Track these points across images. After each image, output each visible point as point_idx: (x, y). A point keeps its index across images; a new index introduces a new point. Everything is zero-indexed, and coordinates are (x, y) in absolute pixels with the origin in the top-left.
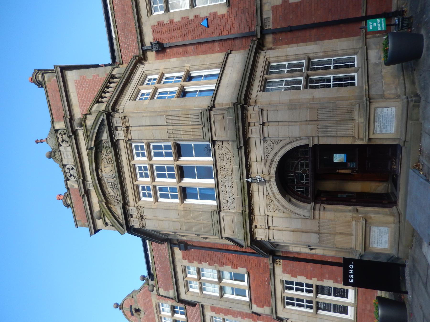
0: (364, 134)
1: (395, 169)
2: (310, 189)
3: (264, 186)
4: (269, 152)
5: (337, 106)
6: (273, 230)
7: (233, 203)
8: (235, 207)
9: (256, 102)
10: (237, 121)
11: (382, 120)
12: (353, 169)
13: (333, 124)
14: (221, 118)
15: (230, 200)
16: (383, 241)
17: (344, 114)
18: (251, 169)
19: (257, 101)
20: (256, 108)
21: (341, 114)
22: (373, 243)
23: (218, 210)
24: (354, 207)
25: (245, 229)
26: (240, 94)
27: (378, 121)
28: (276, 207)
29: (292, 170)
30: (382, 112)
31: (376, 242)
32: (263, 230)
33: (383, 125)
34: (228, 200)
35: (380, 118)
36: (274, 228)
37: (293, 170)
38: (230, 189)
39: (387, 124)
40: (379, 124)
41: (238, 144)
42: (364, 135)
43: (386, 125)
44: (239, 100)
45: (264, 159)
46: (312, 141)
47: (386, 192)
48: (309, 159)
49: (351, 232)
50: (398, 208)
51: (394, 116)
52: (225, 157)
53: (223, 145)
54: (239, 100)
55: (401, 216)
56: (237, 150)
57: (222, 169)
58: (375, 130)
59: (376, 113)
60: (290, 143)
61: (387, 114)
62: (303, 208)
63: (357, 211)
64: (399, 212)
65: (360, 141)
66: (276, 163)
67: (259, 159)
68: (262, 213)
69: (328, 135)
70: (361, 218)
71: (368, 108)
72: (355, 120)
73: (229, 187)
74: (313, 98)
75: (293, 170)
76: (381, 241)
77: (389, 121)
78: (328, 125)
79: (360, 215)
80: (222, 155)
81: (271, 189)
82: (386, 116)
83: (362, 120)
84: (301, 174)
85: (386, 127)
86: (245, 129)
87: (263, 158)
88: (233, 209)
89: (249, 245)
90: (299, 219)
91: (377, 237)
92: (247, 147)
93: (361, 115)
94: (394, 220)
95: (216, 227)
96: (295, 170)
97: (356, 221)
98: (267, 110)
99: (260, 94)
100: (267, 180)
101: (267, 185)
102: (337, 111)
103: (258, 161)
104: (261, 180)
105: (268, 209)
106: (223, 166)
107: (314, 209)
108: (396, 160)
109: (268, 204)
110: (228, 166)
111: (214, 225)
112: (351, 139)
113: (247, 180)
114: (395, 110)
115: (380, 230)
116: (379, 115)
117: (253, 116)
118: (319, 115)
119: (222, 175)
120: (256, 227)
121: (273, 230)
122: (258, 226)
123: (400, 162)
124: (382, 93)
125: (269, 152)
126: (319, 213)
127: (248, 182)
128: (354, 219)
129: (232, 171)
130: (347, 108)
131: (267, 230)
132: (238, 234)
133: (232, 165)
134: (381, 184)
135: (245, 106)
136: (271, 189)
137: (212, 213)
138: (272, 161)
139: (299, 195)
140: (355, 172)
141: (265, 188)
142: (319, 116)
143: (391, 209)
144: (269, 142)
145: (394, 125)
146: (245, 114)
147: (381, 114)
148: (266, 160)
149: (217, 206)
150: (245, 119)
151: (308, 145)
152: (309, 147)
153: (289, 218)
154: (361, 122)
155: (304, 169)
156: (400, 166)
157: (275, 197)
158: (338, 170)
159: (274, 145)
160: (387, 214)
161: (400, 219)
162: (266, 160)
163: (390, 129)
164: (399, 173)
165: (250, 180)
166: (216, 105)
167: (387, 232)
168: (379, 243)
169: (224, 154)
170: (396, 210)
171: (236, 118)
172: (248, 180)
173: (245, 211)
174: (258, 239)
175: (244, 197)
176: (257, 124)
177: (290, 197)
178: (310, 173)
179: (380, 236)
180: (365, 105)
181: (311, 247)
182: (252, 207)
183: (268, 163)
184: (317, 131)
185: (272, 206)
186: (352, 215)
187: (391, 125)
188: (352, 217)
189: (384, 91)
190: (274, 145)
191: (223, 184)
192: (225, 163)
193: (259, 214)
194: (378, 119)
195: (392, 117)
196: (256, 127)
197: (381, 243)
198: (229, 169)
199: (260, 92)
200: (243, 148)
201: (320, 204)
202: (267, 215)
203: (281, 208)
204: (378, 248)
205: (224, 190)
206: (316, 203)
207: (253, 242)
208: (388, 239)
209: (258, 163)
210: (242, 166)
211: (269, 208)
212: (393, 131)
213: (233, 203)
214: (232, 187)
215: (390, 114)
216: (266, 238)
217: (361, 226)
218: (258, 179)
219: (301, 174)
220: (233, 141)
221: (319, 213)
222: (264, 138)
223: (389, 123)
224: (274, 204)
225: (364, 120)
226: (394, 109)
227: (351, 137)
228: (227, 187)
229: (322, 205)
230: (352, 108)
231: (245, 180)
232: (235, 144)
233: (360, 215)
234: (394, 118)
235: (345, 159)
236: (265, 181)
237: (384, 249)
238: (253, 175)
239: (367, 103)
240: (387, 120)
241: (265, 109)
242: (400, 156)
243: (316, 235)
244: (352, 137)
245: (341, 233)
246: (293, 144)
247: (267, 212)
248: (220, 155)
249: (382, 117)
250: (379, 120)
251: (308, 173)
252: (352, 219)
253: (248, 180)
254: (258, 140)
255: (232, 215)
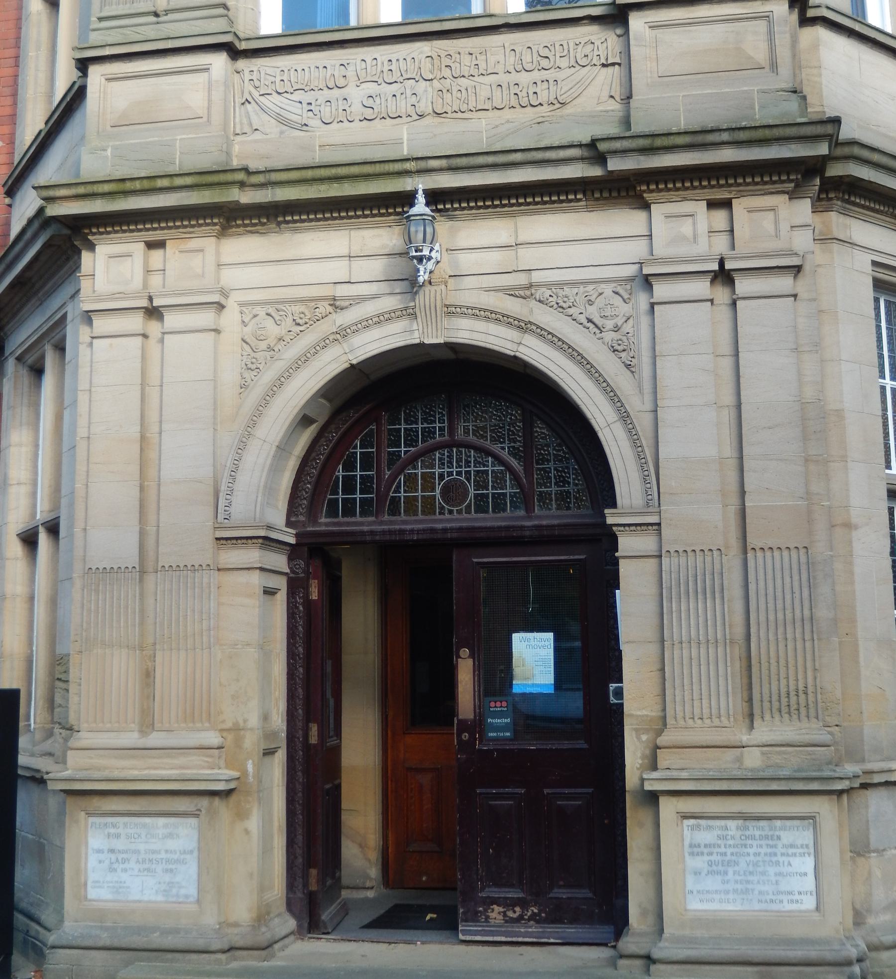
0: (684, 775)
1: (487, 918)
2: (362, 524)
3: (384, 287)
4: (571, 311)
5: (819, 639)
6: (145, 336)
7: (282, 121)
8: (257, 136)
9: (824, 239)
10: (742, 136)
11: (751, 851)
12: (478, 725)
13: (731, 626)
14: (750, 58)
15: (296, 108)
16: (124, 877)
17: (783, 675)
18: (475, 218)
19: (836, 246)
20: (802, 241)
21: (782, 662)
22: (112, 831)
23: (240, 40)
24: (284, 735)
25: (146, 184)
26: (876, 157)
27: (747, 833)
28: (270, 349)
29: (460, 431)
30: (791, 851)
31: (119, 844)
32: (137, 283)
33: (729, 857)
34: (297, 96)
35: (763, 842)
36: (152, 342)
37: (460, 434)
38: (356, 109)
39: (730, 875)
40: (733, 838)
41: (618, 145)
42: (675, 774)
43: (726, 873)
44: (846, 150)
45: (530, 286)
46: (636, 525)
47: (345, 881)
48: (522, 513)
49: (157, 725)
50: (292, 938)
51: (774, 907)
52: (537, 75)
53: (604, 65)
54: (846, 150)
55: (263, 953)
56: (586, 139)
57: (466, 60)
58: (703, 822)
59: (788, 823)
60: (625, 417)
61: (780, 874)
62: (270, 490)
63: (269, 753)
64: (276, 946)
65: (639, 754)
66: (509, 345)
67: (528, 257)
68: (231, 277)
69: (670, 600)
70: (233, 769)
71: (815, 786)
72: (752, 727)
73: (370, 102)
74: (849, 526)
75: (460, 434)
76: (126, 866)
77: (748, 882)
78: (723, 598)
79: (250, 767)
80: (545, 63)
81: (366, 324)
82: (771, 870)
83: (753, 760)
84: (441, 477)
85: (719, 873)
86: (705, 183)
87: (536, 277)
88: (245, 121)
89: (53, 211)
90: (214, 466)
91: (142, 847)
92: (597, 195)
93: (779, 753)
94: (236, 925)
95: (139, 29)
96: (460, 445)
97: (220, 748)
98: (795, 296)
99: (864, 261)
100: (420, 299)
101: (390, 303)
102: (795, 639)
103: (522, 251)
104: (422, 268)
105: (258, 310)
106: (483, 66)
107: (268, 542)
108: (532, 923)
109: (281, 307)
110: (484, 93)
111: (153, 19)
112: (654, 714)
113: (416, 191)
114: (803, 907)
115: (183, 862)
116: (779, 838)
117: (767, 221)
118: (777, 553)
119: (437, 62)
120: (151, 245)
121: (145, 336)
122: (156, 255)
123: (520, 939)
124: (873, 847)
125: (571, 311)
126: (248, 569)
127: (408, 199)
128: (230, 737)
129: (460, 115)
130: (810, 689)
131: (144, 303)
132: (109, 150)
133: (490, 114)
134: (374, 855)
135: (818, 181)
136: (366, 324)
137: (221, 11)
138: (524, 326)
139: (327, 468)
140: (465, 736)
141: (373, 289)
142: (768, 554)
143: (283, 908)
144: (625, 309)
145: (730, 907)
146: (774, 183)
147: (784, 846)
148: (528, 293)
149: (253, 35)
150: (749, 180)
151: (614, 505)
152: (606, 511)
153: (215, 417)
154: (742, 754)
155: (438, 496)
156: (503, 939)
157: (323, 344)
158: (470, 657)
159: (609, 336)
160: (262, 889)
161: (245, 953)
162: (528, 293)
163: (708, 892)
164: (468, 938)
165: (420, 207)
166: (811, 34)
167: (174, 891)
168: (113, 857)
169: (550, 75)
170: (283, 933)
171: (760, 134)
172: (421, 199)
173: (242, 185)
174: (86, 256)
175: (321, 180)
176: (721, 245)
177: (321, 421)
178: (448, 520)
179: (151, 861)
180: (827, 773)
181: (43, 539)
182: (264, 224)
183: (513, 306)
184: (689, 549)
185: (273, 330)
186: (251, 729)
187: (727, 892)
188: (237, 730)
189: (880, 852)
190: (609, 336)
191: (386, 69)
192: (503, 78)
193: (225, 259)
194: (757, 833)
195: (768, 897)
196: (703, 239)
197: (115, 866)
198: (472, 98)
199: (875, 263)
200: (595, 172)
201: (288, 571)
202: (223, 302)
203: (268, 376)
204: (86, 854)
205: (350, 73)
206: (293, 552)
207: (66, 231)
208: (140, 901)
209: (510, 253)
210: (494, 166)
211: (261, 311)
212: (695, 905)
213: (282, 121)
214: (369, 113)
215: (783, 887)
216: (100, 300)
217: (195, 771)
218: (426, 252)
219: (441, 477)
220: (627, 122)
221: (248, 569)
222: (647, 282)
223: (739, 886)
224: (287, 339)
225: (752, 770)
226: (809, 903)
227: (664, 710)
228: (371, 88)
229: (281, 583)
230: (812, 712)
231: (420, 184)
232: (613, 130)
233: (250, 767)
234: (763, 906)
235: (528, 690)
236: (412, 285)
237: (86, 884)
238: (443, 226)
239: (841, 779)
240: (751, 873)
241: (802, 286)
242: (552, 940)
243: (131, 558)
244: (665, 717)
245: (148, 676)
246: (619, 431)
247: (242, 304)
248: (545, 53)
249: (769, 850)
250: (753, 838)
251: (451, 512)
252: (228, 730)
253: (421, 199)
254: (637, 250)
255: (217, 118)
